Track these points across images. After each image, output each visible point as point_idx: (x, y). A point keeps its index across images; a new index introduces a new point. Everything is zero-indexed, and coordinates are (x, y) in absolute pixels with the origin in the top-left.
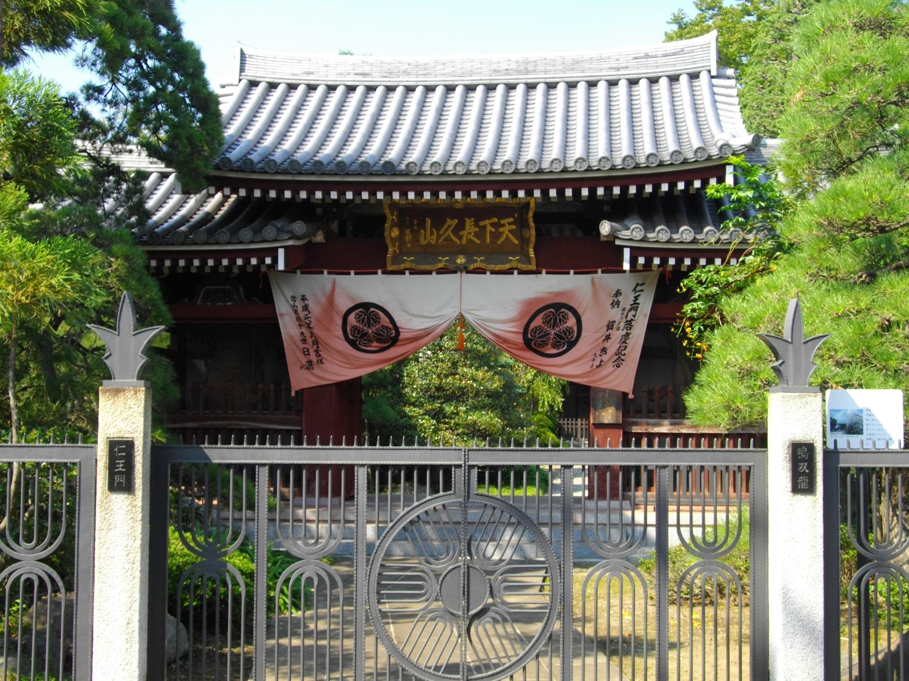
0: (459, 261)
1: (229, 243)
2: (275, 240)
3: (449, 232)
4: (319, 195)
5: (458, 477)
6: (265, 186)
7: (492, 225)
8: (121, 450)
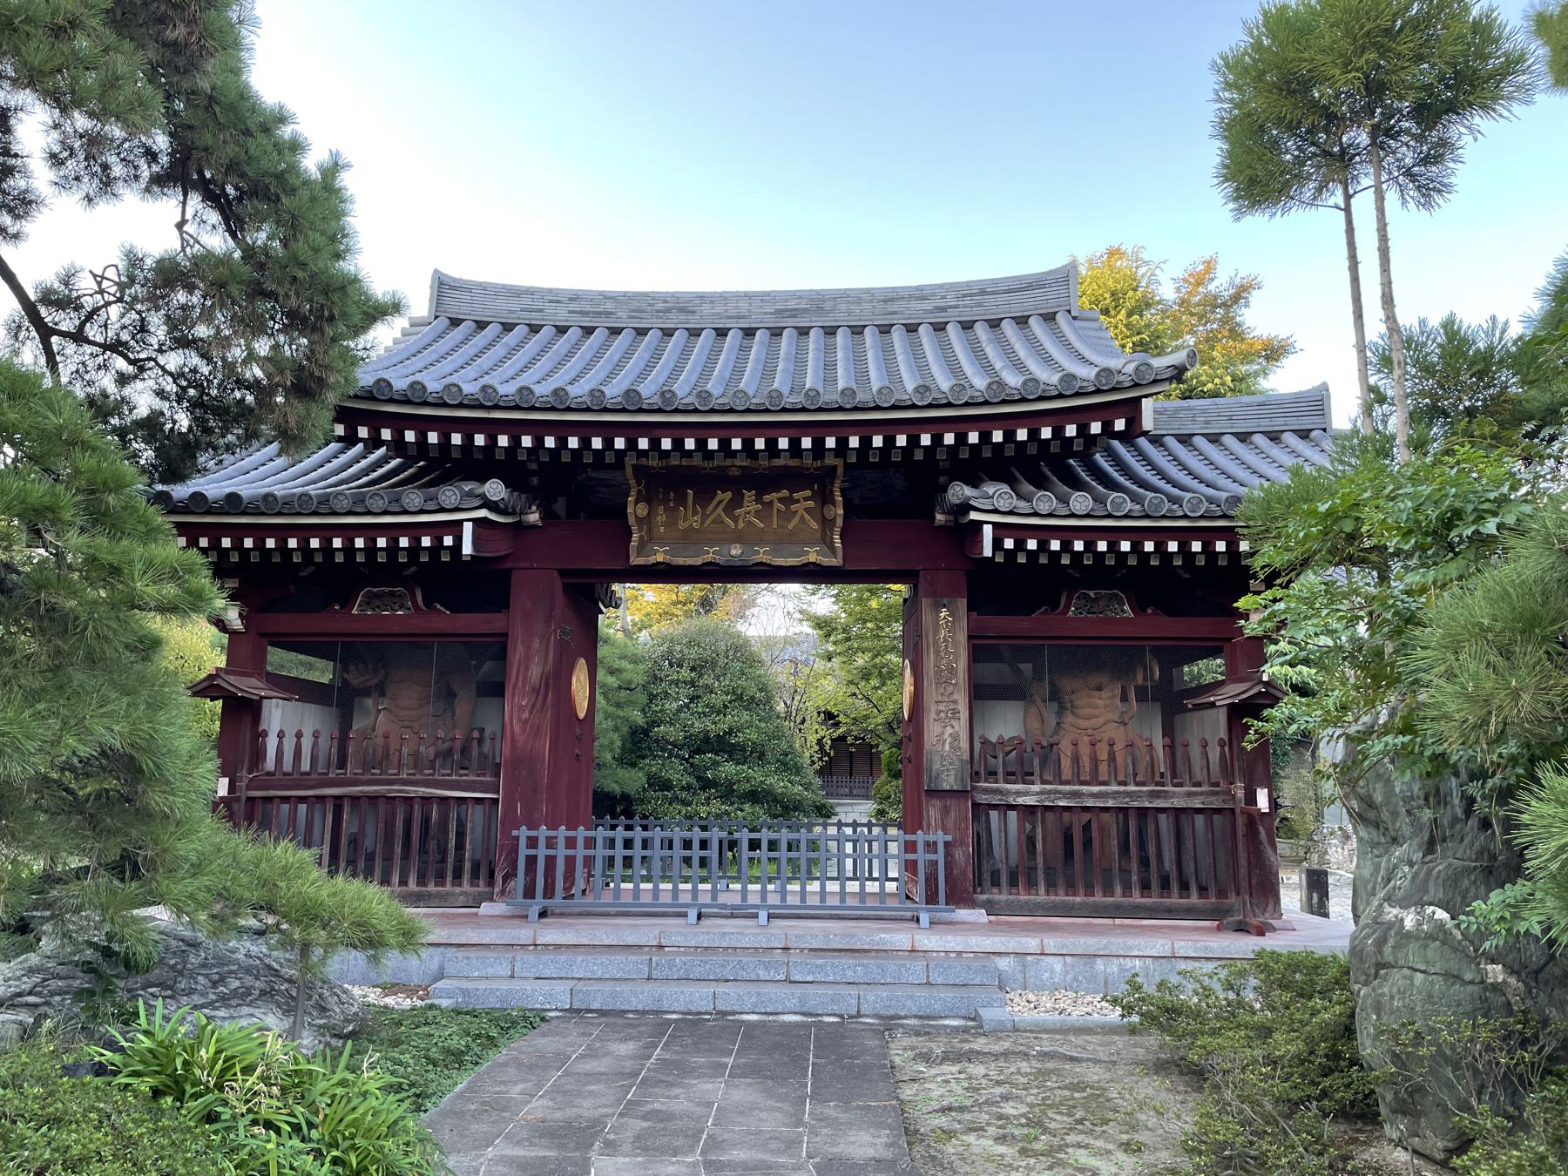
0: (733, 552)
2: (457, 510)
3: (720, 510)
7: (781, 500)
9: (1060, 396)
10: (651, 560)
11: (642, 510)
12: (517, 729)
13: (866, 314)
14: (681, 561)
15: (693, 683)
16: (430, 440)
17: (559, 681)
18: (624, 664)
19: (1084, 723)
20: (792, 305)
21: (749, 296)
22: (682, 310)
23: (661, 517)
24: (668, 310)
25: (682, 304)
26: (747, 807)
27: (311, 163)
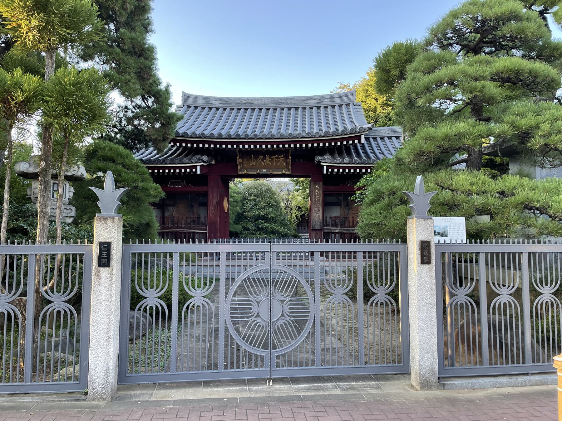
1: (179, 164)
4: (212, 146)
5: (267, 256)
6: (192, 142)
8: (105, 247)
9: (341, 135)
10: (243, 173)
11: (241, 160)
12: (211, 215)
13: (300, 104)
14: (251, 173)
15: (255, 200)
16: (191, 147)
17: (220, 204)
18: (235, 195)
19: (354, 212)
20: (279, 101)
21: (267, 99)
22: (250, 103)
23: (245, 162)
24: (246, 103)
25: (250, 101)
26: (271, 235)
27: (162, 87)
